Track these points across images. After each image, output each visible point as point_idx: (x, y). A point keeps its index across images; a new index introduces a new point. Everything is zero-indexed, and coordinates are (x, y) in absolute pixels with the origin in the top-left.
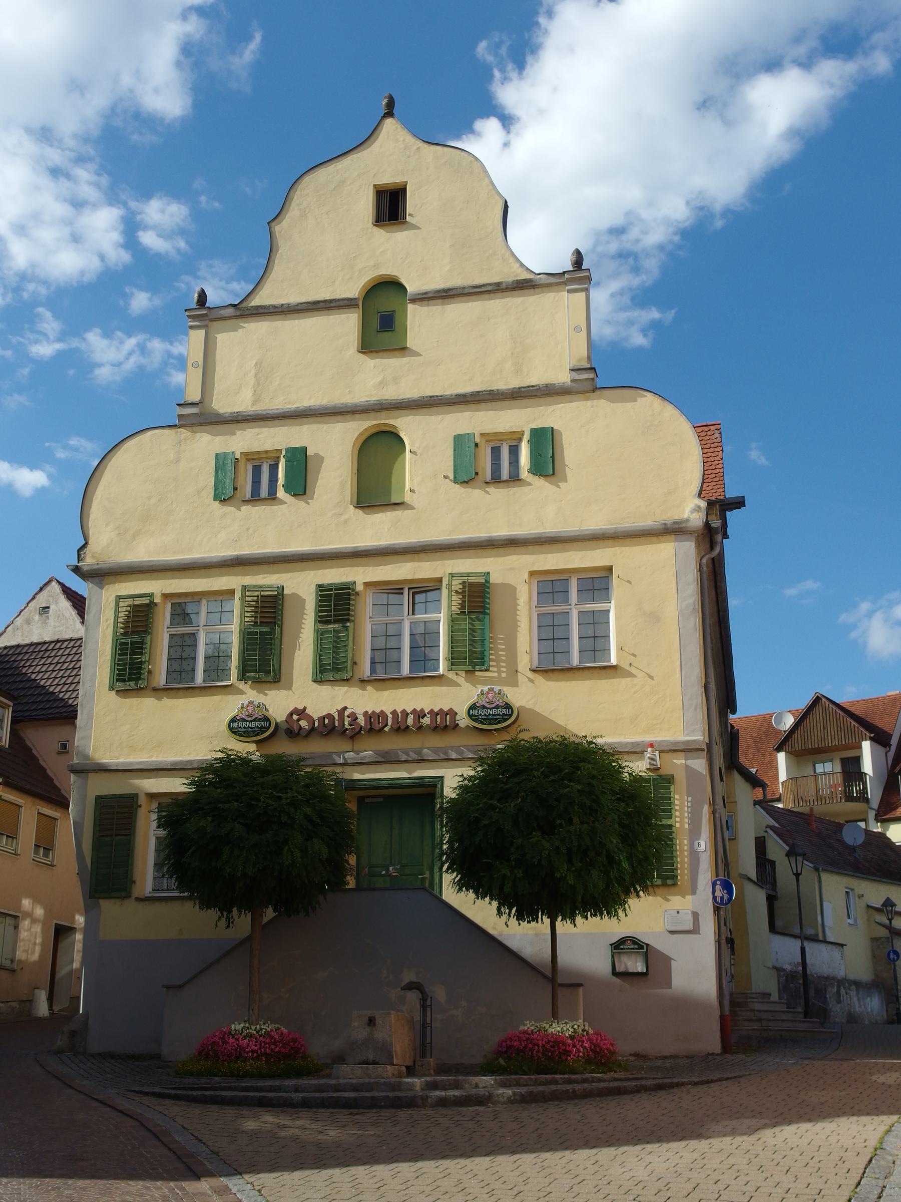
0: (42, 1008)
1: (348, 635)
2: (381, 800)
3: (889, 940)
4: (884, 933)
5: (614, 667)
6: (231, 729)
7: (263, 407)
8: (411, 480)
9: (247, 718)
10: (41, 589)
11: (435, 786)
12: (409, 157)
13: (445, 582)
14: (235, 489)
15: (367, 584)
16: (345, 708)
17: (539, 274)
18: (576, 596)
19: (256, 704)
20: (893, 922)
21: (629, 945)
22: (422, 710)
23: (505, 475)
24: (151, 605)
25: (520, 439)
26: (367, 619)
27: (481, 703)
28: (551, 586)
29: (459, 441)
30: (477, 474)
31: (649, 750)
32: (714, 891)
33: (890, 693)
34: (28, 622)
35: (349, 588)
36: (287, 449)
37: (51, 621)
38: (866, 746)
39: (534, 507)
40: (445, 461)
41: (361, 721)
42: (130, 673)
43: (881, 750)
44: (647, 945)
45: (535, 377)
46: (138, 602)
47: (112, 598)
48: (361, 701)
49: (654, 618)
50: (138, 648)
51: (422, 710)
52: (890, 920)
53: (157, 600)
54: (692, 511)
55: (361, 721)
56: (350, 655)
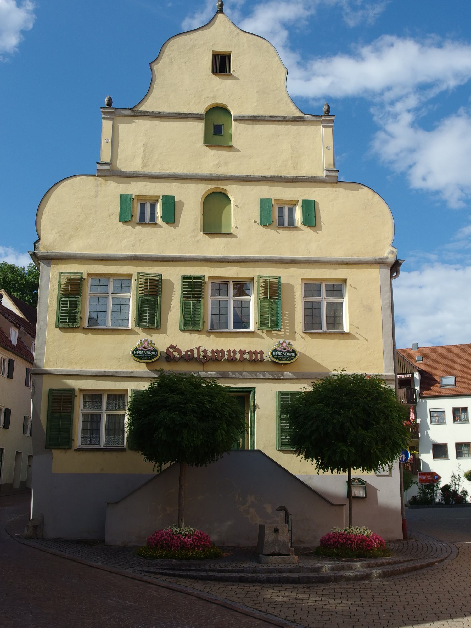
1: (200, 306)
5: (348, 334)
6: (134, 355)
7: (148, 170)
8: (236, 221)
12: (233, 38)
13: (255, 280)
14: (133, 216)
15: (89, 274)
16: (201, 346)
19: (149, 341)
26: (209, 298)
28: (311, 288)
36: (163, 196)
39: (300, 243)
40: (255, 213)
42: (69, 317)
44: (366, 482)
46: (73, 276)
48: (209, 343)
49: (369, 309)
50: (74, 304)
53: (85, 276)
54: (389, 253)
56: (202, 317)
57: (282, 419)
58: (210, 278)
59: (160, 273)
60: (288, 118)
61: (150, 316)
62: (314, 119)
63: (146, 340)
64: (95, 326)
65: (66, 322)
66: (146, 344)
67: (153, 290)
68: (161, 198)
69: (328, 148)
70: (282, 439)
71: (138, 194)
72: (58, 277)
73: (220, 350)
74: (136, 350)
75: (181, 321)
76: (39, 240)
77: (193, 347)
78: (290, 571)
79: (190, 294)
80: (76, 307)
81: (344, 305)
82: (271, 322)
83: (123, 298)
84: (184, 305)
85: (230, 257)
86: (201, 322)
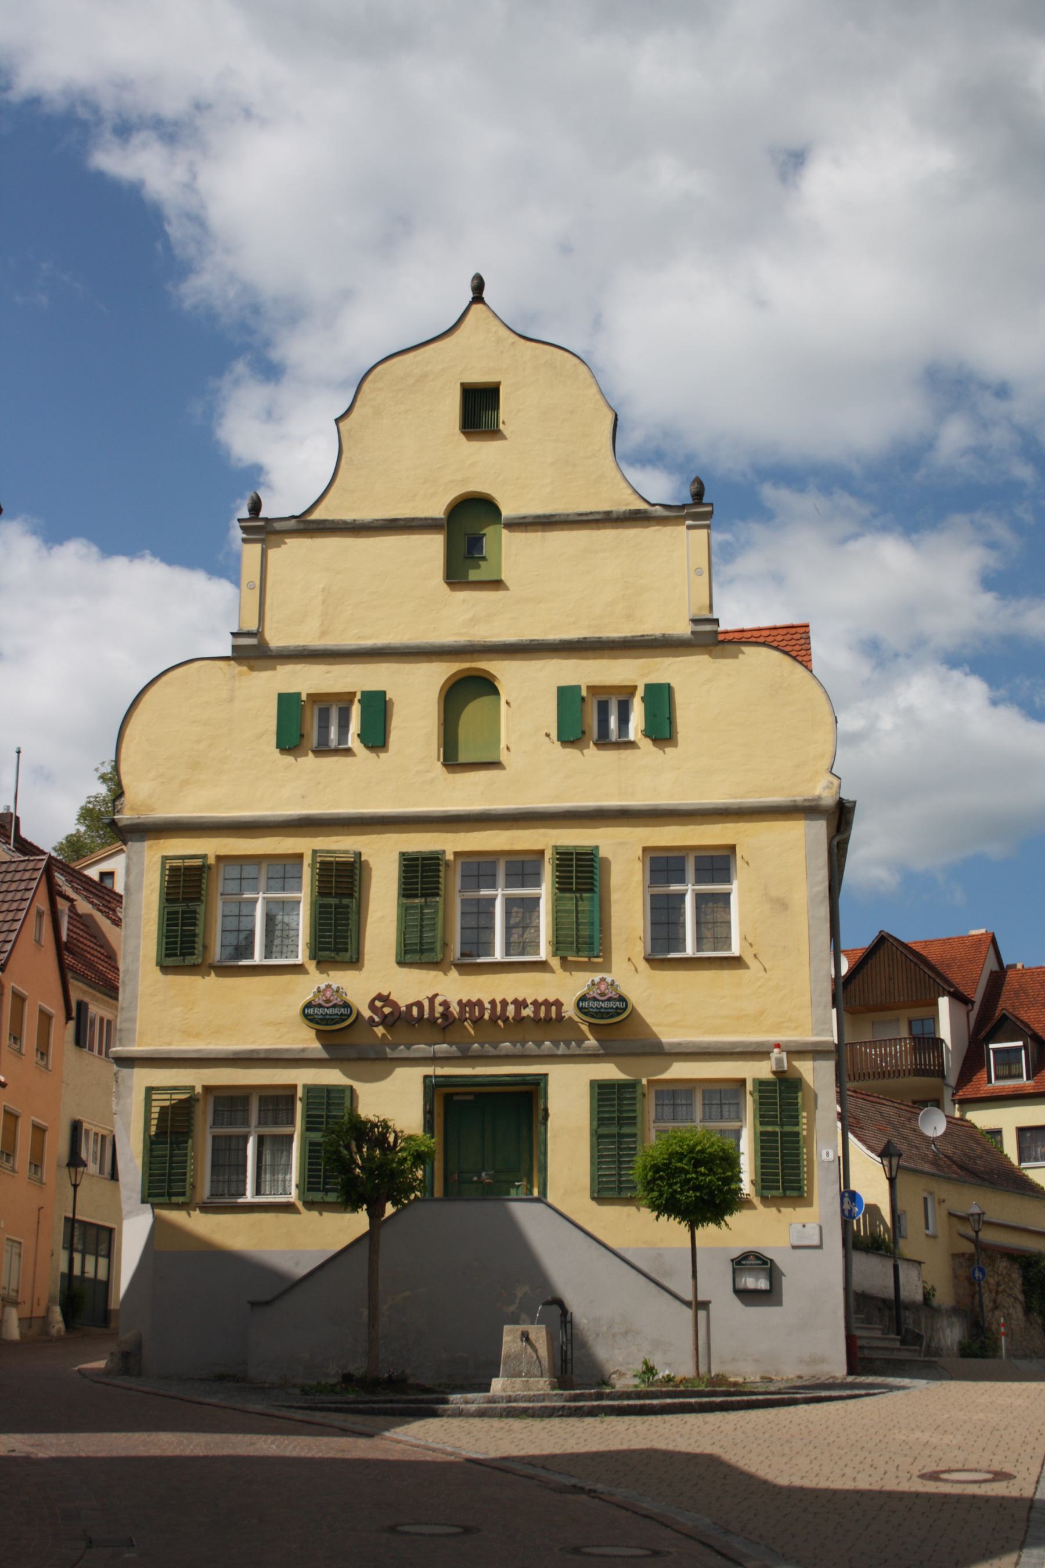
1: (436, 912)
2: (471, 1098)
9: (324, 1004)
11: (538, 1084)
12: (502, 352)
14: (302, 736)
15: (219, 858)
16: (437, 995)
17: (654, 505)
18: (692, 877)
19: (334, 987)
20: (980, 1234)
21: (752, 1261)
22: (524, 1000)
23: (614, 736)
26: (455, 895)
28: (663, 866)
30: (584, 733)
31: (776, 1050)
32: (842, 1204)
33: (974, 932)
35: (438, 858)
36: (363, 693)
38: (944, 1002)
39: (640, 776)
42: (181, 947)
43: (962, 1009)
44: (771, 1260)
46: (189, 863)
47: (157, 859)
48: (453, 988)
49: (781, 905)
51: (524, 1000)
52: (977, 1232)
54: (824, 789)
55: (455, 1009)
56: (440, 935)
57: (600, 1136)
58: (457, 854)
59: (357, 848)
60: (614, 515)
61: (337, 938)
62: (666, 513)
63: (329, 986)
64: (234, 963)
65: (175, 955)
68: (640, 693)
69: (698, 572)
70: (600, 1176)
71: (312, 691)
73: (474, 1000)
74: (309, 1005)
75: (398, 944)
77: (423, 996)
78: (530, 1399)
79: (417, 889)
80: (195, 925)
81: (732, 897)
82: (583, 940)
83: (288, 902)
84: (404, 912)
85: (495, 810)
86: (439, 946)
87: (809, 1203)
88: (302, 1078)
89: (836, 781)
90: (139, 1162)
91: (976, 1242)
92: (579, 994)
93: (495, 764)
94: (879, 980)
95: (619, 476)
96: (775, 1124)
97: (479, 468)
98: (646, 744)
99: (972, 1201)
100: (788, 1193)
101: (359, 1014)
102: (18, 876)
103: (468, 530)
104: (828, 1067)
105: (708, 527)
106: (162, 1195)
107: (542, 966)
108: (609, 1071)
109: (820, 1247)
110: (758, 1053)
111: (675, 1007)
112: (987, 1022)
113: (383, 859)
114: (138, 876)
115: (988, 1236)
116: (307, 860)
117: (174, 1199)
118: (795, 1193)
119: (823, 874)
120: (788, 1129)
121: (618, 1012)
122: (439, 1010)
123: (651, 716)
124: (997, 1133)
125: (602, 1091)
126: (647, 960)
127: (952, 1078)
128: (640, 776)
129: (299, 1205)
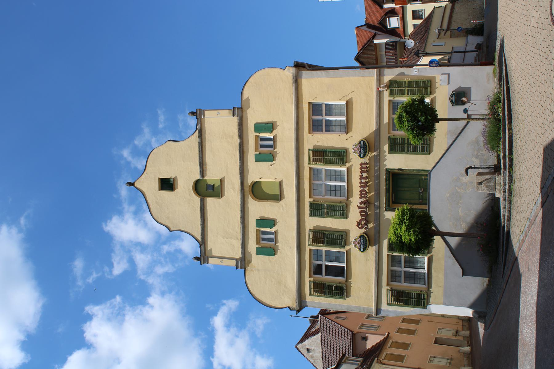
0: (467, 349)
3: (451, 31)
4: (449, 32)
5: (347, 102)
6: (364, 251)
7: (240, 236)
8: (271, 179)
10: (300, 351)
13: (311, 166)
15: (310, 197)
18: (319, 117)
24: (314, 282)
25: (258, 136)
26: (325, 198)
27: (358, 153)
28: (316, 127)
29: (257, 160)
34: (312, 357)
37: (313, 348)
38: (375, 41)
39: (285, 135)
40: (265, 165)
41: (363, 200)
42: (341, 292)
43: (377, 36)
45: (235, 131)
46: (312, 287)
47: (310, 297)
48: (356, 200)
50: (330, 287)
53: (312, 279)
55: (363, 200)
56: (337, 204)
57: (408, 151)
61: (339, 238)
66: (356, 149)
67: (320, 236)
68: (257, 134)
69: (218, 114)
72: (313, 297)
74: (360, 250)
76: (289, 307)
78: (505, 185)
82: (340, 156)
87: (435, 77)
88: (385, 252)
89: (287, 68)
90: (412, 309)
91: (447, 31)
92: (358, 157)
93: (281, 184)
94: (367, 58)
95: (188, 140)
96: (405, 90)
97: (185, 185)
98: (275, 132)
99: (434, 30)
100: (429, 85)
101: (364, 233)
102: (325, 324)
103: (205, 190)
104: (387, 71)
105: (204, 110)
106: (424, 302)
107: (349, 170)
108: (386, 148)
109: (449, 75)
110: (380, 94)
111: (364, 125)
112: (382, 28)
113: (312, 223)
114: (317, 302)
115: (445, 27)
116: (311, 248)
117: (426, 297)
118: (429, 83)
119: (319, 72)
120: (407, 85)
121: (364, 143)
122: (363, 205)
123: (265, 131)
124: (414, 25)
125: (392, 150)
126: (347, 133)
127: (397, 39)
128: (285, 135)
129: (429, 255)
